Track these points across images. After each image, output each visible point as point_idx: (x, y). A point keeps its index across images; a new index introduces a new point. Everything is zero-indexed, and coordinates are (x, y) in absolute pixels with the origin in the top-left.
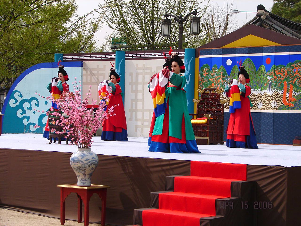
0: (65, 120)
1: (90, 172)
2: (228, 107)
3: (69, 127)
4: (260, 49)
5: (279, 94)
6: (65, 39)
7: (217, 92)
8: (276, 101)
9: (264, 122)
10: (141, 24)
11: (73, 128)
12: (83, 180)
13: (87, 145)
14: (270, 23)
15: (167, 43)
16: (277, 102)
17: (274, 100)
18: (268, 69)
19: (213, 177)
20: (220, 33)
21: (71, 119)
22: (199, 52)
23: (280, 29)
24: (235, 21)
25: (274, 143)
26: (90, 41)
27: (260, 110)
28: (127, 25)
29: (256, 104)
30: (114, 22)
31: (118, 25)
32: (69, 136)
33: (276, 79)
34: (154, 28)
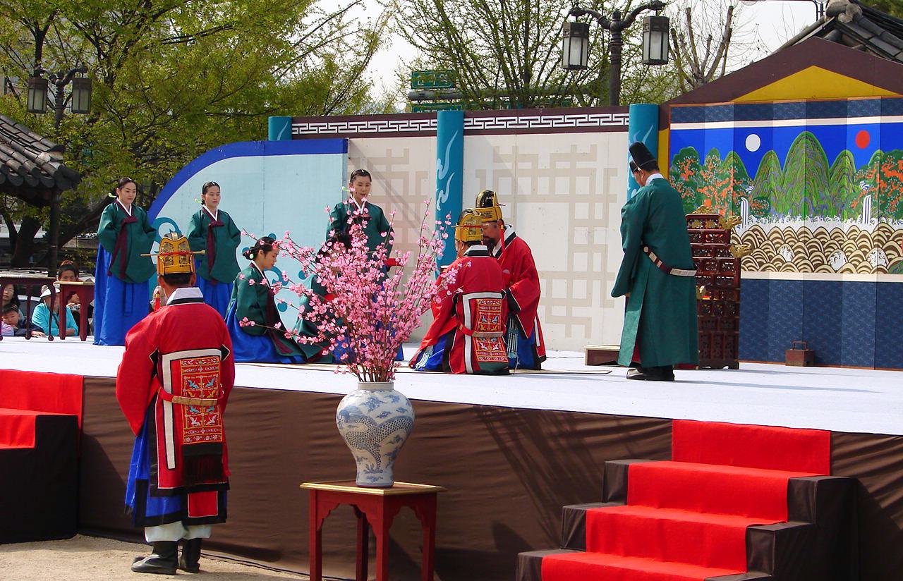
0: (321, 305)
1: (391, 448)
2: (749, 266)
3: (332, 325)
4: (839, 107)
5: (893, 231)
6: (290, 77)
7: (720, 225)
8: (885, 251)
9: (851, 306)
10: (495, 31)
11: (346, 328)
13: (383, 374)
14: (865, 35)
15: (565, 84)
16: (887, 252)
17: (878, 246)
18: (861, 162)
19: (735, 464)
20: (709, 58)
21: (340, 302)
22: (670, 113)
23: (892, 51)
24: (752, 25)
25: (878, 365)
26: (357, 81)
27: (838, 273)
28: (454, 37)
29: (827, 257)
30: (418, 29)
31: (430, 35)
32: (333, 348)
33: (884, 189)
34: (530, 45)
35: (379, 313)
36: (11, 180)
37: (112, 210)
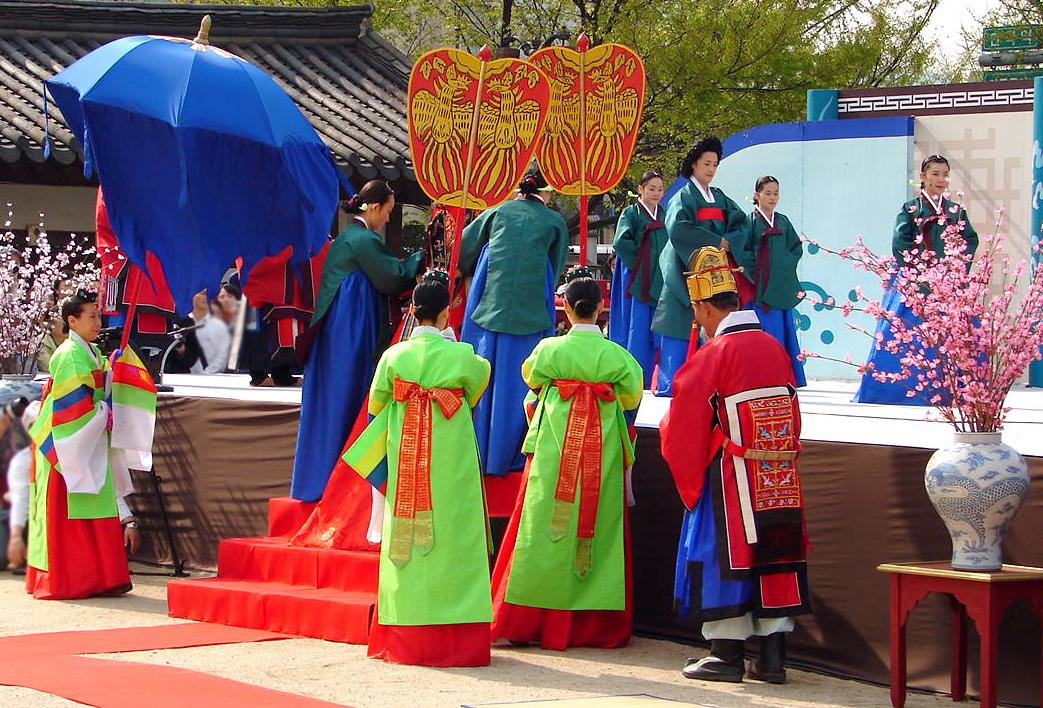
1: (999, 519)
3: (920, 357)
6: (823, 42)
11: (938, 361)
12: (974, 549)
13: (987, 421)
21: (930, 329)
26: (916, 41)
32: (922, 388)
35: (983, 341)
37: (631, 214)
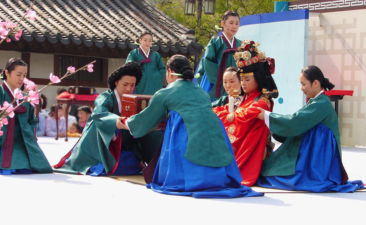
36: (162, 49)
